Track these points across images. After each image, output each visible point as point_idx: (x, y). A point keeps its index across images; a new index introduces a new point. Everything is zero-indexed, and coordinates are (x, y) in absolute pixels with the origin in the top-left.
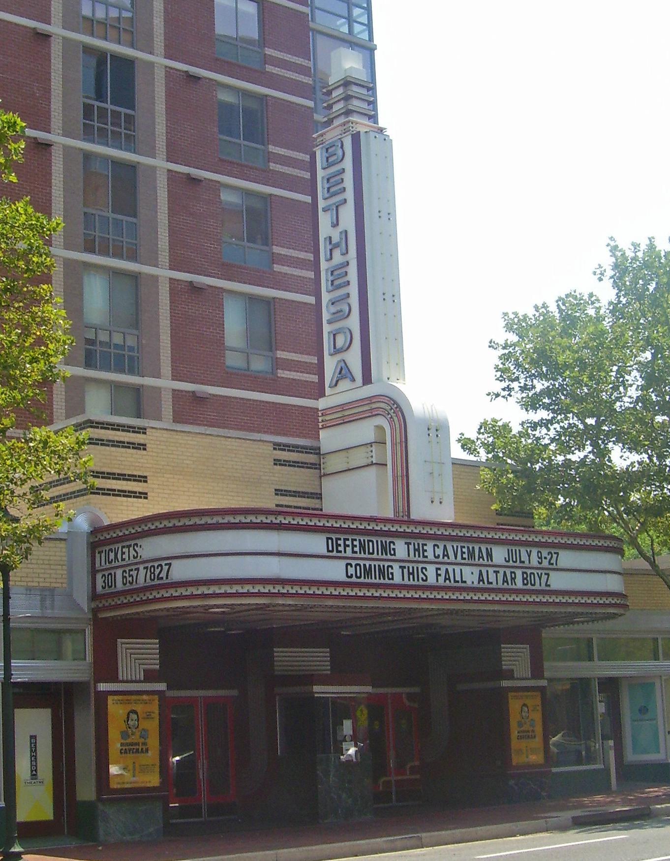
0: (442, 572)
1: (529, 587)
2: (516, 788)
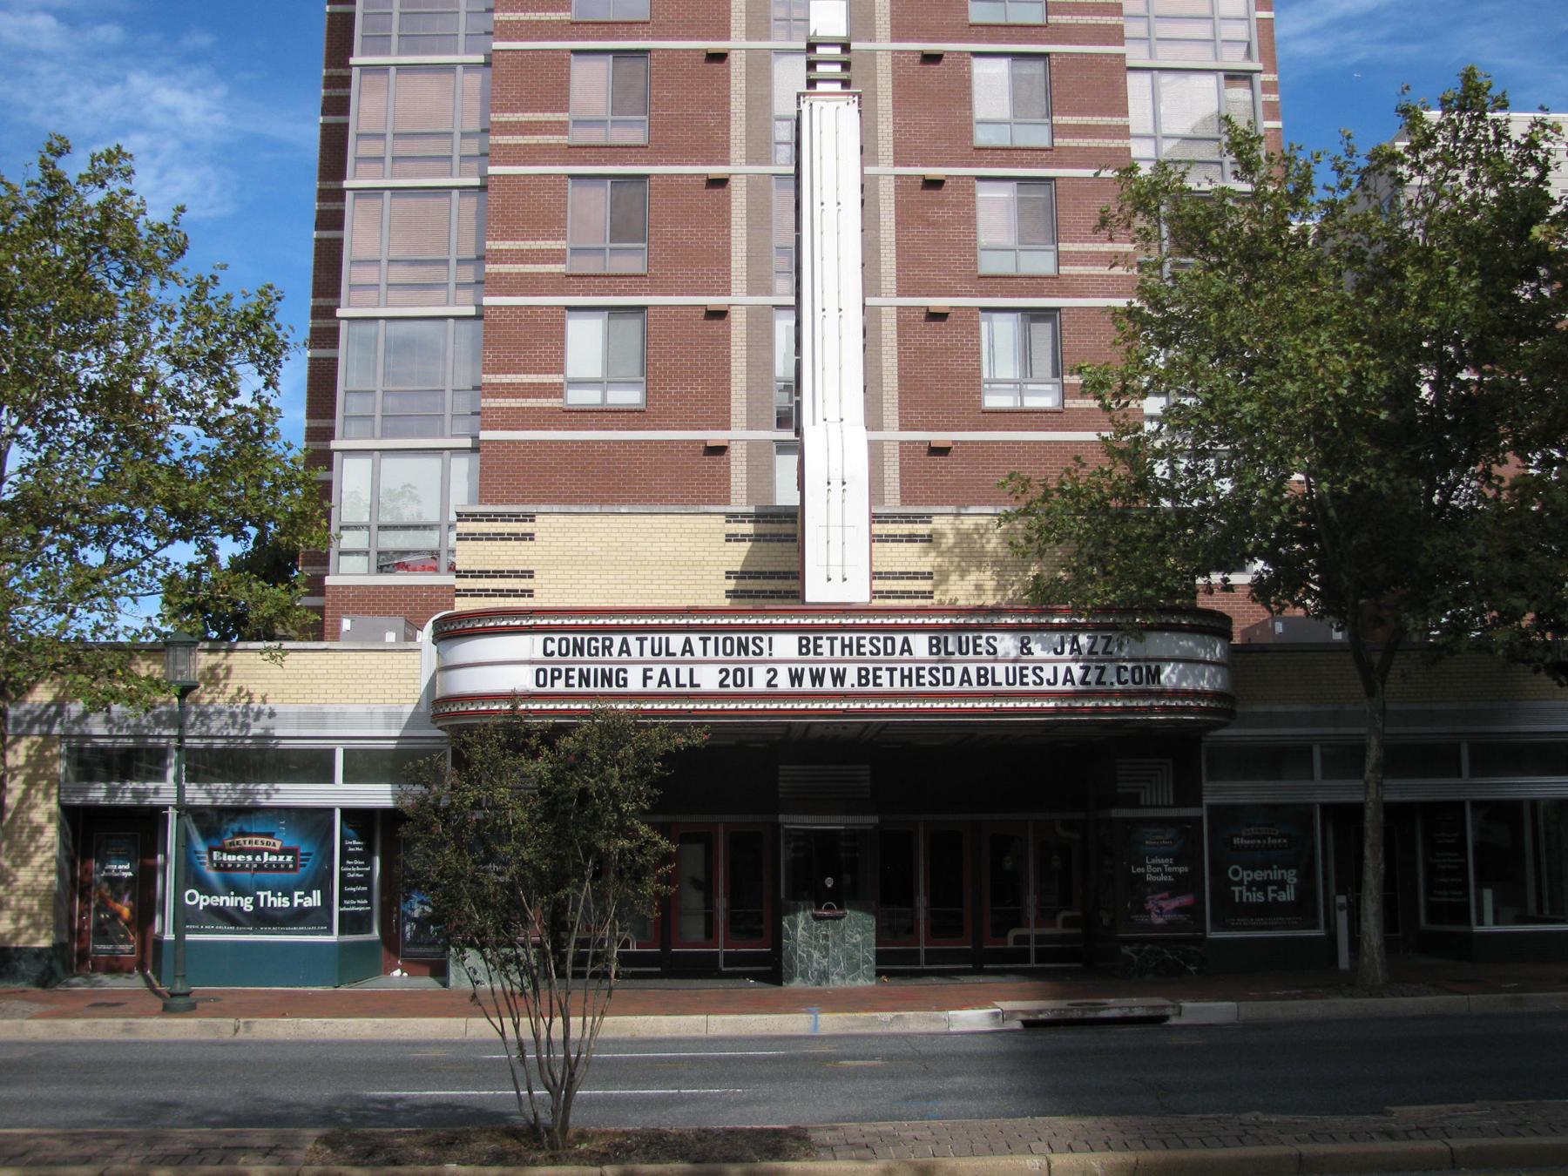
0: (656, 673)
2: (1136, 958)
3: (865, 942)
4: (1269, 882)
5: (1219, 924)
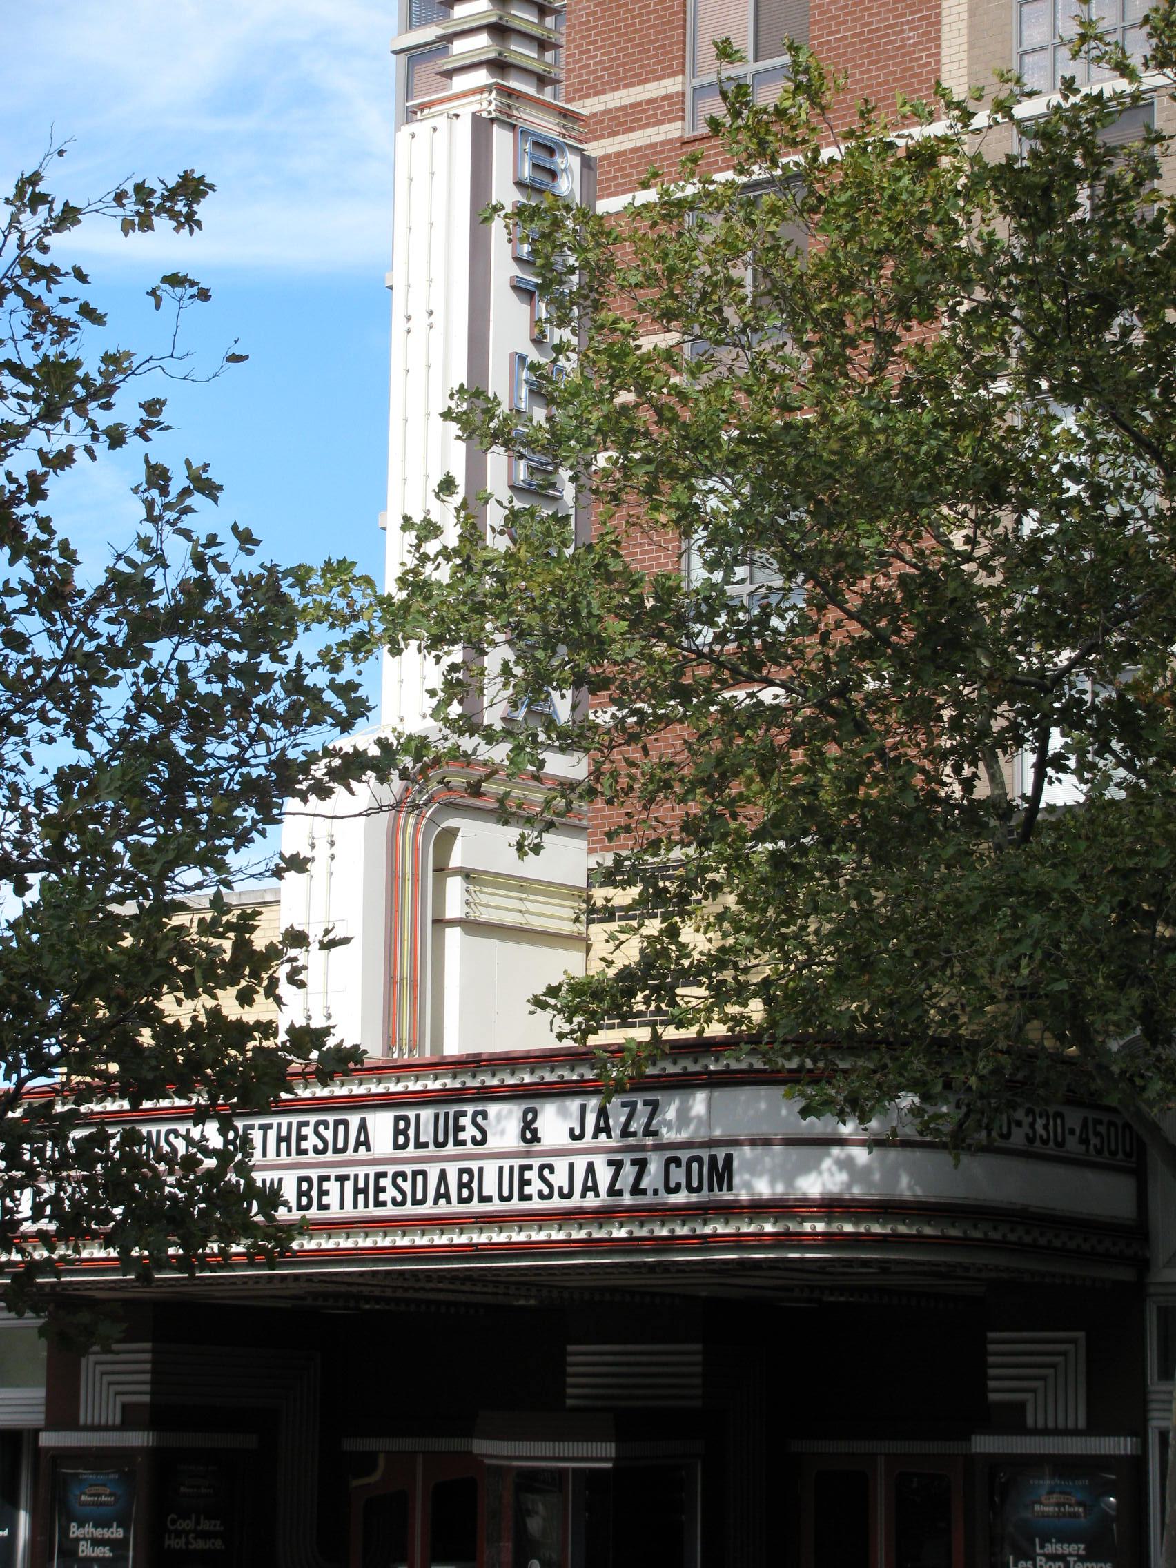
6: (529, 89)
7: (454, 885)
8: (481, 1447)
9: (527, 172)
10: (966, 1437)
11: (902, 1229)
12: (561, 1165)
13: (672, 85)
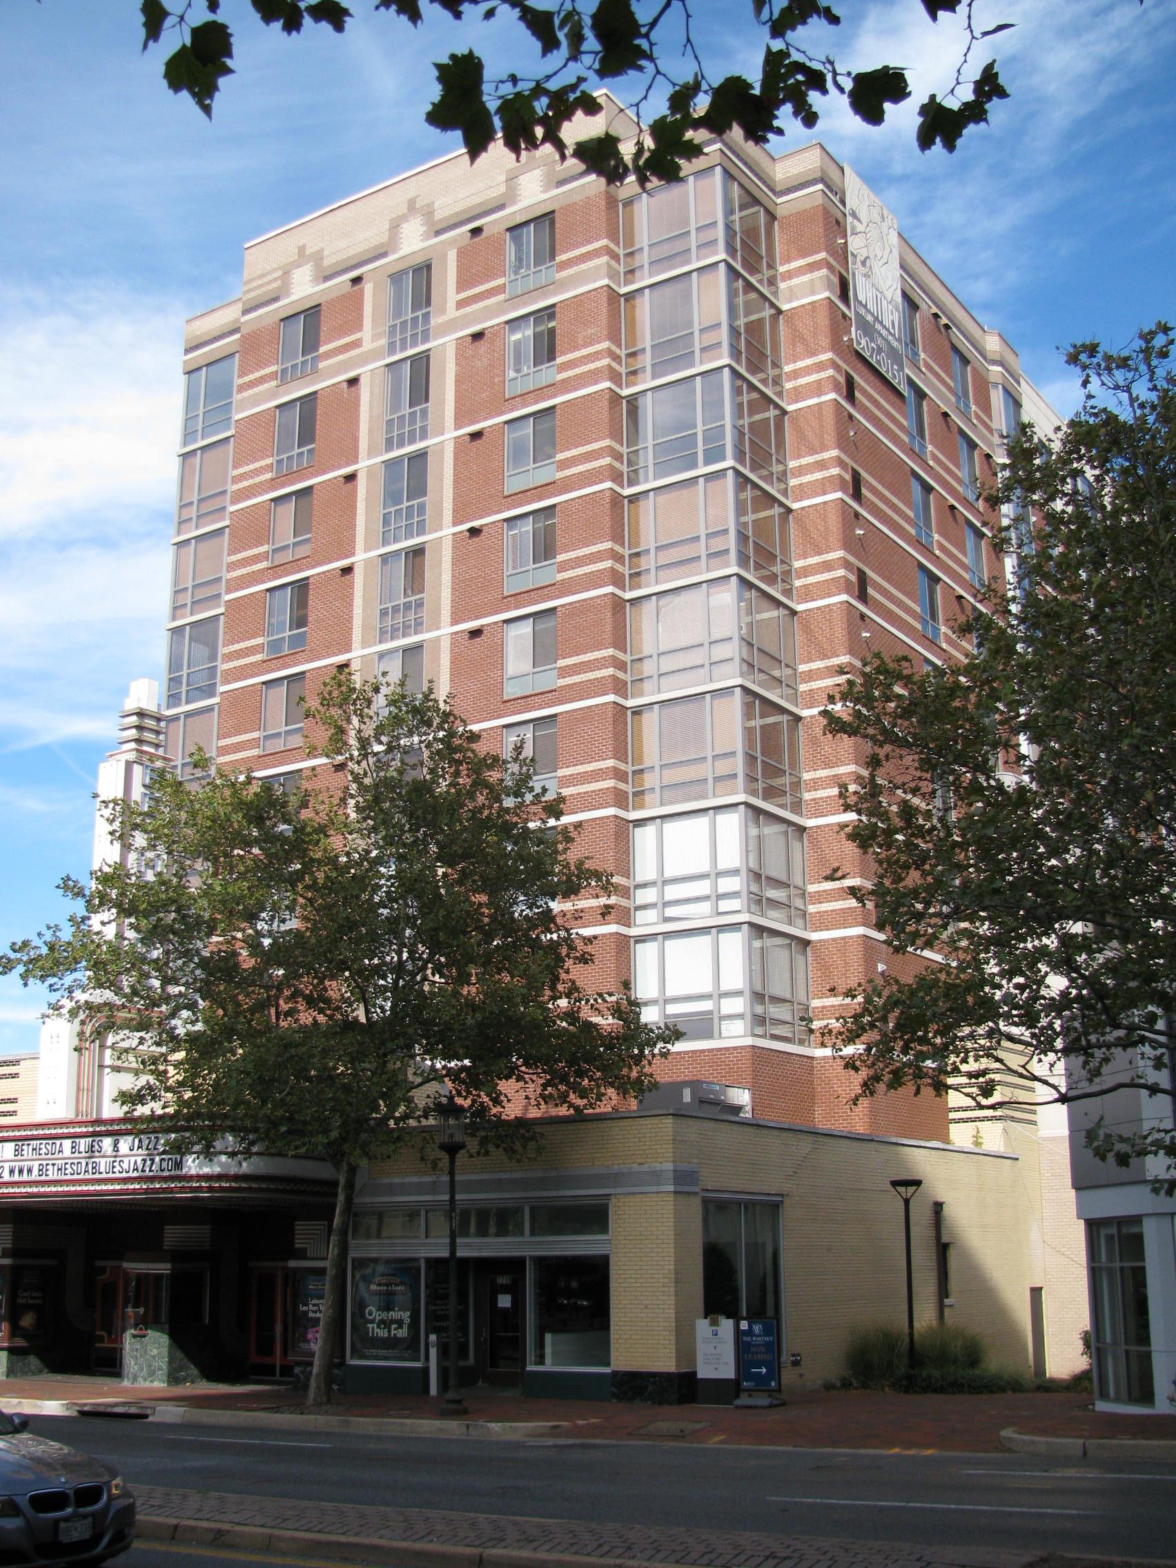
1: (44, 1178)
3: (160, 1356)
4: (392, 1321)
5: (356, 1353)
6: (152, 750)
7: (108, 1052)
8: (126, 1265)
9: (147, 781)
10: (287, 1260)
11: (224, 1185)
12: (126, 1160)
13: (255, 735)
